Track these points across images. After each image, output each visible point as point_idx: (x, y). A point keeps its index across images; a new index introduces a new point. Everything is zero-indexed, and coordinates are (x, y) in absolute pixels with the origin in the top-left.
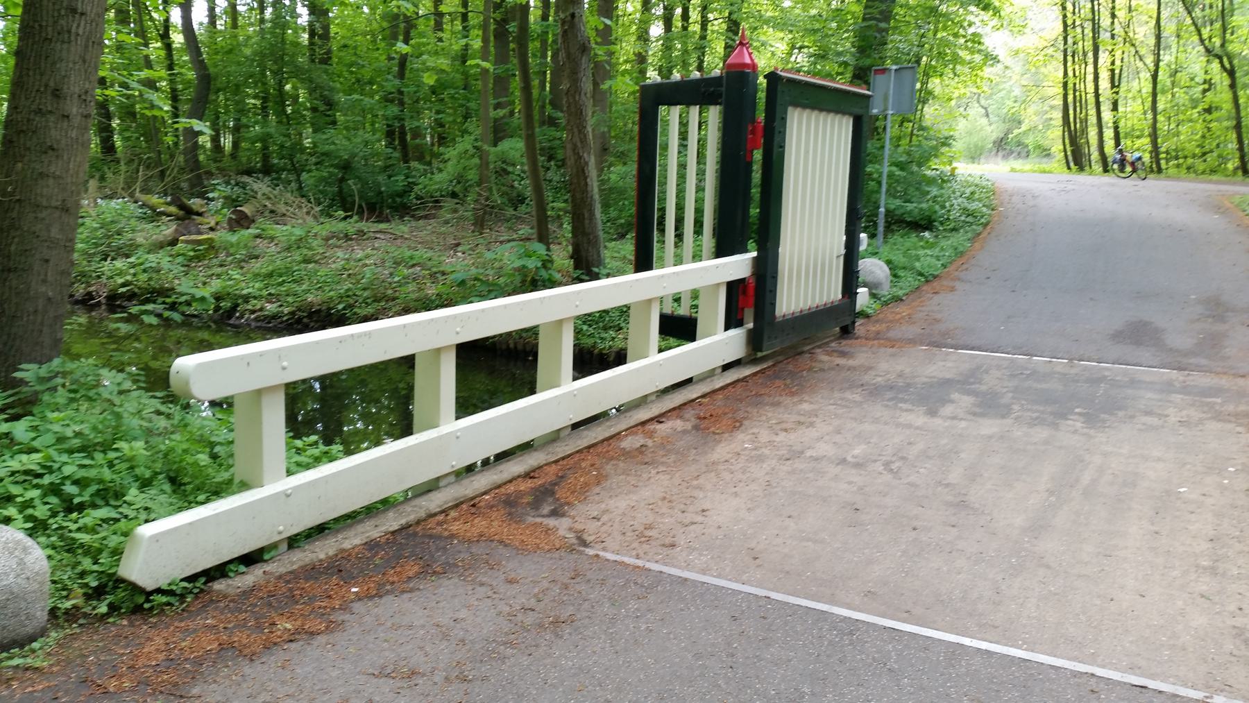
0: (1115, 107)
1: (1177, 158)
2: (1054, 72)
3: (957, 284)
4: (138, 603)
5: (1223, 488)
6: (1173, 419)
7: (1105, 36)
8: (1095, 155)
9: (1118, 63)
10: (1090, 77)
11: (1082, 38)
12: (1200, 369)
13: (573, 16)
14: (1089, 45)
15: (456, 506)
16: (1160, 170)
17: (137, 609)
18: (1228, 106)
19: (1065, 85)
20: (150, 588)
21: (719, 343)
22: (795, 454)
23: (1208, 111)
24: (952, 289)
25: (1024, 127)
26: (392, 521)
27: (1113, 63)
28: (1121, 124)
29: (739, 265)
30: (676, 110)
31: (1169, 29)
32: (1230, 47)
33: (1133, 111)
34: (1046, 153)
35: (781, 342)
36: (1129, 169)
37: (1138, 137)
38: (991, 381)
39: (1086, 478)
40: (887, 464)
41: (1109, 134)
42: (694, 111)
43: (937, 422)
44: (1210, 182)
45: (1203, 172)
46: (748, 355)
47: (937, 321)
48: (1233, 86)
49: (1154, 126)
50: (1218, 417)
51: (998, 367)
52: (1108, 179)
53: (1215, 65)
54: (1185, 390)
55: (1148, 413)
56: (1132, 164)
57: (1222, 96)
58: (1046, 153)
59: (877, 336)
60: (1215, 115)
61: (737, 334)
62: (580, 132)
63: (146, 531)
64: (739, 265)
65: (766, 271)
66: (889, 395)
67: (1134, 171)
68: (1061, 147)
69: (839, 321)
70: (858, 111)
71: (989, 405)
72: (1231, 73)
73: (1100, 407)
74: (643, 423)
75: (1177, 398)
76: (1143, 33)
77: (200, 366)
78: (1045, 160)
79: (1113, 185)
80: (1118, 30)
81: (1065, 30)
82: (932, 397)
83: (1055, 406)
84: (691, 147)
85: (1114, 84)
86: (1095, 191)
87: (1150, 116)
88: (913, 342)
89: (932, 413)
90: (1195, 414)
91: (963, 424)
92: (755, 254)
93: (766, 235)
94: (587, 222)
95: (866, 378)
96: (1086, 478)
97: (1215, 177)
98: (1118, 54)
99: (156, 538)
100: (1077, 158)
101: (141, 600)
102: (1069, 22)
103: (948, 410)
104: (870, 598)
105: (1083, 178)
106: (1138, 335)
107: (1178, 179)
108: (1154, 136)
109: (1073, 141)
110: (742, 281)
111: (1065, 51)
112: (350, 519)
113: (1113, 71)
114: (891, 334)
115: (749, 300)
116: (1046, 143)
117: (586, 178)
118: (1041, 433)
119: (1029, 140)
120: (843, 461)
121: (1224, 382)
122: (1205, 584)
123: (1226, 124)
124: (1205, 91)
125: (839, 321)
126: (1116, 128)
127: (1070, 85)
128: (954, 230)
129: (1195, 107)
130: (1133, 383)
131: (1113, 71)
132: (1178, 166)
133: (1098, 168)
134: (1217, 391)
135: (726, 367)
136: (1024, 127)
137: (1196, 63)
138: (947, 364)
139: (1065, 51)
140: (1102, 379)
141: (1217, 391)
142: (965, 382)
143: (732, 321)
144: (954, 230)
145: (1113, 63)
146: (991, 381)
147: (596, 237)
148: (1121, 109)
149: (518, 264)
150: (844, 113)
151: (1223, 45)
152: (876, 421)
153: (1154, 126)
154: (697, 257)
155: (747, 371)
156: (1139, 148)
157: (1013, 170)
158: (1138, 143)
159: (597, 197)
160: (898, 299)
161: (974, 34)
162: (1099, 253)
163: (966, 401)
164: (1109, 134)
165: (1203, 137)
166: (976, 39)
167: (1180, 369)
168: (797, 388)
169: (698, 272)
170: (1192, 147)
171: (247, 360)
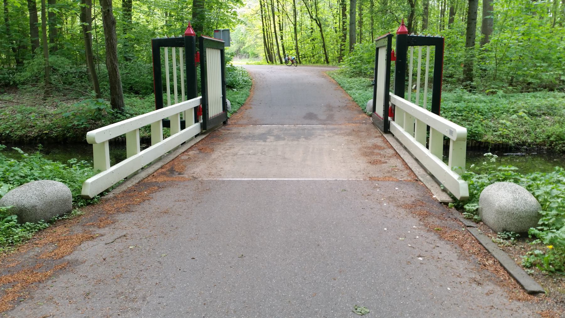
0: (282, 39)
1: (305, 57)
2: (259, 24)
3: (252, 106)
4: (88, 201)
5: (342, 148)
6: (326, 136)
7: (276, 10)
8: (277, 57)
9: (281, 20)
10: (272, 26)
11: (268, 10)
12: (329, 124)
13: (108, 10)
14: (271, 13)
15: (149, 176)
16: (300, 63)
17: (88, 204)
18: (320, 38)
19: (263, 29)
20: (91, 197)
21: (193, 128)
22: (235, 154)
23: (313, 40)
24: (251, 108)
25: (246, 45)
26: (135, 181)
27: (280, 21)
28: (285, 45)
29: (196, 101)
30: (166, 49)
31: (298, 8)
32: (319, 16)
33: (288, 39)
34: (256, 56)
35: (212, 127)
36: (290, 62)
37: (291, 50)
38: (275, 132)
39: (311, 150)
40: (261, 153)
41: (281, 48)
42: (174, 49)
43: (267, 143)
44: (317, 66)
45: (314, 63)
46: (202, 131)
47: (251, 118)
48: (321, 31)
49: (297, 46)
50: (337, 134)
51: (276, 129)
52: (284, 66)
53: (314, 22)
54: (327, 129)
55: (320, 135)
56: (292, 61)
57: (317, 34)
58: (256, 56)
59: (235, 124)
60: (316, 41)
61: (198, 124)
62: (113, 54)
63: (89, 181)
64: (196, 101)
65: (204, 102)
66: (250, 138)
67: (293, 63)
68: (264, 54)
69: (223, 119)
70: (222, 48)
71: (278, 138)
72: (320, 25)
73: (308, 136)
74: (183, 153)
75: (326, 131)
76: (289, 8)
77: (97, 133)
78: (256, 59)
79: (286, 69)
80: (280, 8)
81: (261, 8)
82: (263, 137)
83: (297, 136)
84: (174, 62)
85: (281, 30)
86: (280, 72)
87: (295, 42)
88: (247, 124)
89: (265, 141)
90: (331, 135)
91: (275, 143)
92: (201, 97)
93: (204, 91)
94: (117, 89)
95: (240, 135)
96: (311, 150)
97: (318, 65)
98: (281, 17)
99: (92, 183)
100: (270, 58)
101: (89, 201)
102: (263, 4)
103: (268, 140)
104: (274, 176)
105: (274, 66)
106: (311, 117)
107: (307, 66)
108: (297, 49)
109: (269, 52)
110: (197, 107)
111: (262, 16)
112: (119, 184)
113: (280, 24)
114: (239, 123)
115: (201, 112)
116: (256, 52)
117: (116, 72)
118: (295, 143)
119: (249, 51)
120: (249, 154)
121: (336, 126)
122: (343, 164)
123: (320, 44)
124: (312, 32)
125: (223, 119)
126: (283, 46)
127: (265, 30)
128: (241, 88)
129: (309, 38)
130: (313, 129)
131: (280, 24)
132: (306, 60)
133: (278, 62)
134: (335, 129)
135: (196, 136)
136: (246, 45)
137: (308, 22)
138: (261, 129)
139: (262, 16)
140: (305, 129)
141: (335, 129)
142: (269, 133)
143: (196, 121)
144: (241, 88)
145: (280, 21)
146: (275, 132)
147: (121, 95)
148: (284, 38)
149: (96, 107)
150: (218, 49)
151: (316, 16)
152: (251, 145)
153: (297, 46)
154: (180, 100)
155: (204, 137)
156: (292, 54)
157: (247, 64)
158: (291, 52)
159: (120, 79)
160: (235, 112)
161: (234, 12)
162: (291, 94)
163: (272, 138)
164: (281, 48)
165: (313, 49)
166: (235, 14)
167: (324, 124)
168: (222, 139)
169: (180, 106)
170: (309, 53)
171: (104, 132)
